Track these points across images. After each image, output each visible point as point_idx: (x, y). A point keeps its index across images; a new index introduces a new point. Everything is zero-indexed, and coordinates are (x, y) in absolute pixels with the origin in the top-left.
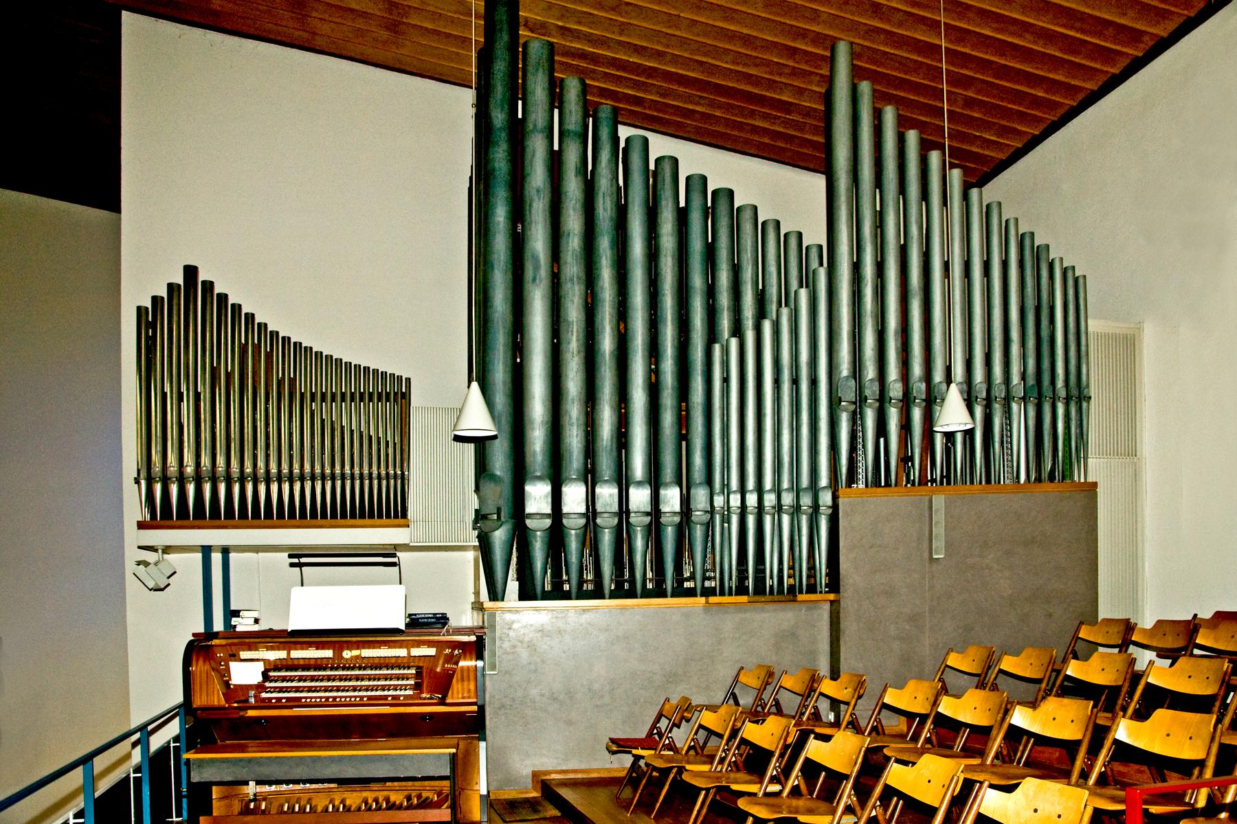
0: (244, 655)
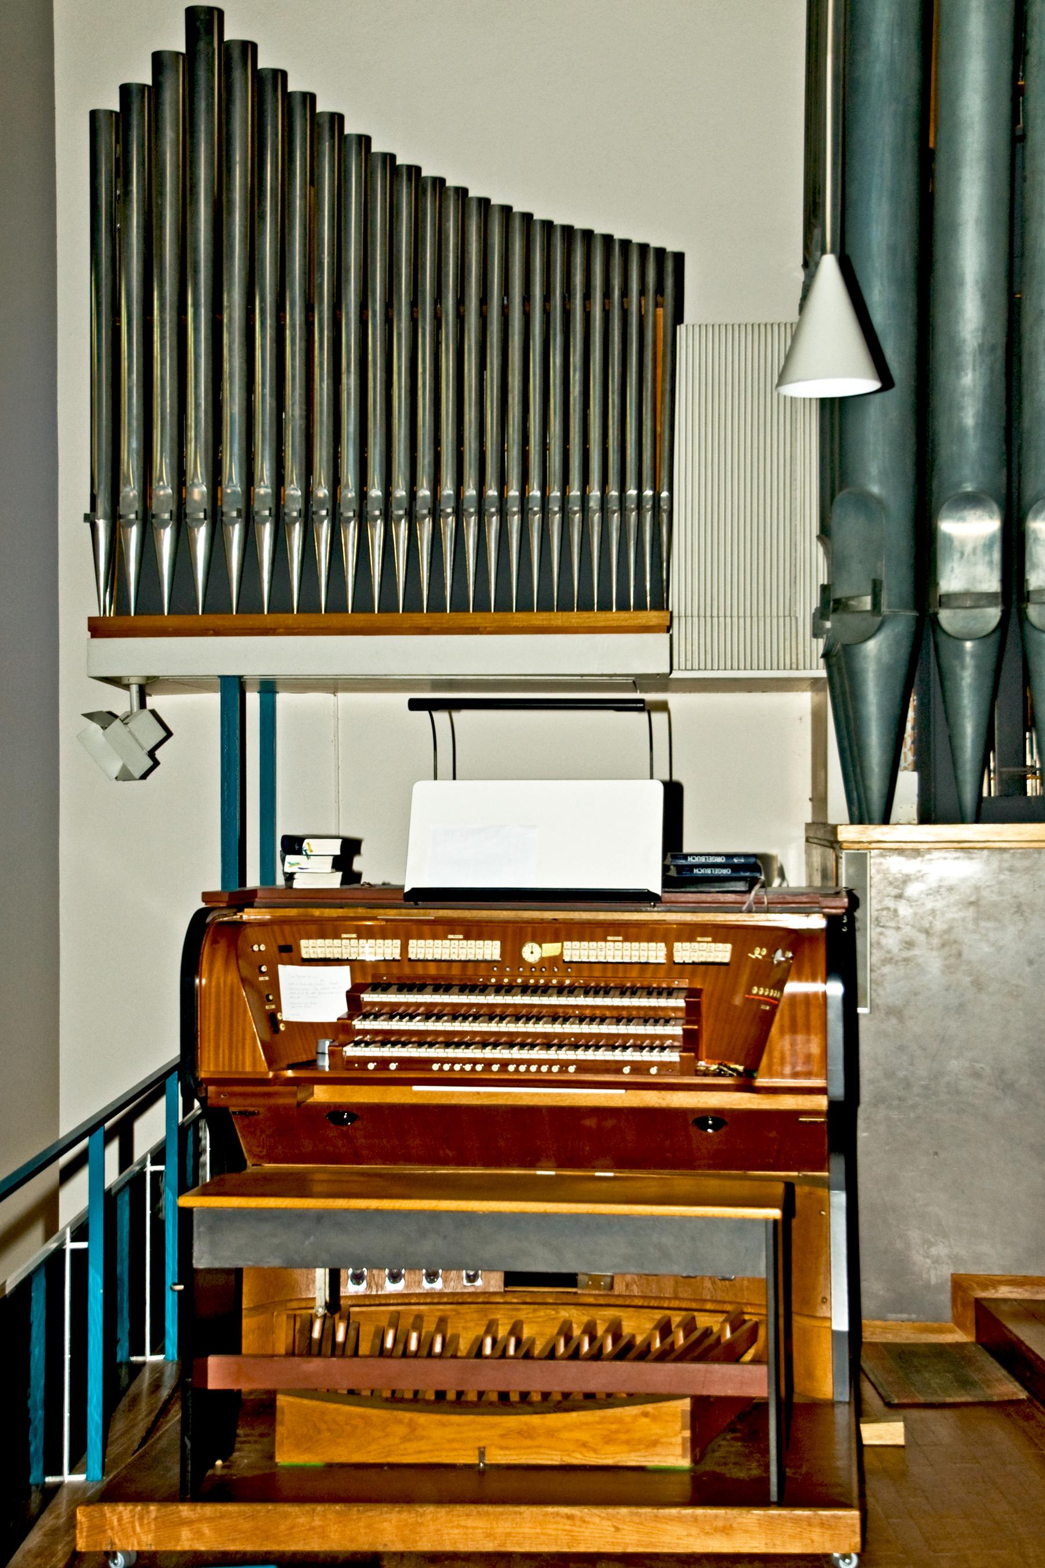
0: (310, 948)
